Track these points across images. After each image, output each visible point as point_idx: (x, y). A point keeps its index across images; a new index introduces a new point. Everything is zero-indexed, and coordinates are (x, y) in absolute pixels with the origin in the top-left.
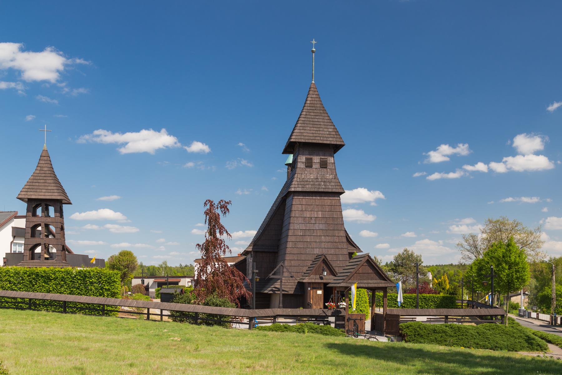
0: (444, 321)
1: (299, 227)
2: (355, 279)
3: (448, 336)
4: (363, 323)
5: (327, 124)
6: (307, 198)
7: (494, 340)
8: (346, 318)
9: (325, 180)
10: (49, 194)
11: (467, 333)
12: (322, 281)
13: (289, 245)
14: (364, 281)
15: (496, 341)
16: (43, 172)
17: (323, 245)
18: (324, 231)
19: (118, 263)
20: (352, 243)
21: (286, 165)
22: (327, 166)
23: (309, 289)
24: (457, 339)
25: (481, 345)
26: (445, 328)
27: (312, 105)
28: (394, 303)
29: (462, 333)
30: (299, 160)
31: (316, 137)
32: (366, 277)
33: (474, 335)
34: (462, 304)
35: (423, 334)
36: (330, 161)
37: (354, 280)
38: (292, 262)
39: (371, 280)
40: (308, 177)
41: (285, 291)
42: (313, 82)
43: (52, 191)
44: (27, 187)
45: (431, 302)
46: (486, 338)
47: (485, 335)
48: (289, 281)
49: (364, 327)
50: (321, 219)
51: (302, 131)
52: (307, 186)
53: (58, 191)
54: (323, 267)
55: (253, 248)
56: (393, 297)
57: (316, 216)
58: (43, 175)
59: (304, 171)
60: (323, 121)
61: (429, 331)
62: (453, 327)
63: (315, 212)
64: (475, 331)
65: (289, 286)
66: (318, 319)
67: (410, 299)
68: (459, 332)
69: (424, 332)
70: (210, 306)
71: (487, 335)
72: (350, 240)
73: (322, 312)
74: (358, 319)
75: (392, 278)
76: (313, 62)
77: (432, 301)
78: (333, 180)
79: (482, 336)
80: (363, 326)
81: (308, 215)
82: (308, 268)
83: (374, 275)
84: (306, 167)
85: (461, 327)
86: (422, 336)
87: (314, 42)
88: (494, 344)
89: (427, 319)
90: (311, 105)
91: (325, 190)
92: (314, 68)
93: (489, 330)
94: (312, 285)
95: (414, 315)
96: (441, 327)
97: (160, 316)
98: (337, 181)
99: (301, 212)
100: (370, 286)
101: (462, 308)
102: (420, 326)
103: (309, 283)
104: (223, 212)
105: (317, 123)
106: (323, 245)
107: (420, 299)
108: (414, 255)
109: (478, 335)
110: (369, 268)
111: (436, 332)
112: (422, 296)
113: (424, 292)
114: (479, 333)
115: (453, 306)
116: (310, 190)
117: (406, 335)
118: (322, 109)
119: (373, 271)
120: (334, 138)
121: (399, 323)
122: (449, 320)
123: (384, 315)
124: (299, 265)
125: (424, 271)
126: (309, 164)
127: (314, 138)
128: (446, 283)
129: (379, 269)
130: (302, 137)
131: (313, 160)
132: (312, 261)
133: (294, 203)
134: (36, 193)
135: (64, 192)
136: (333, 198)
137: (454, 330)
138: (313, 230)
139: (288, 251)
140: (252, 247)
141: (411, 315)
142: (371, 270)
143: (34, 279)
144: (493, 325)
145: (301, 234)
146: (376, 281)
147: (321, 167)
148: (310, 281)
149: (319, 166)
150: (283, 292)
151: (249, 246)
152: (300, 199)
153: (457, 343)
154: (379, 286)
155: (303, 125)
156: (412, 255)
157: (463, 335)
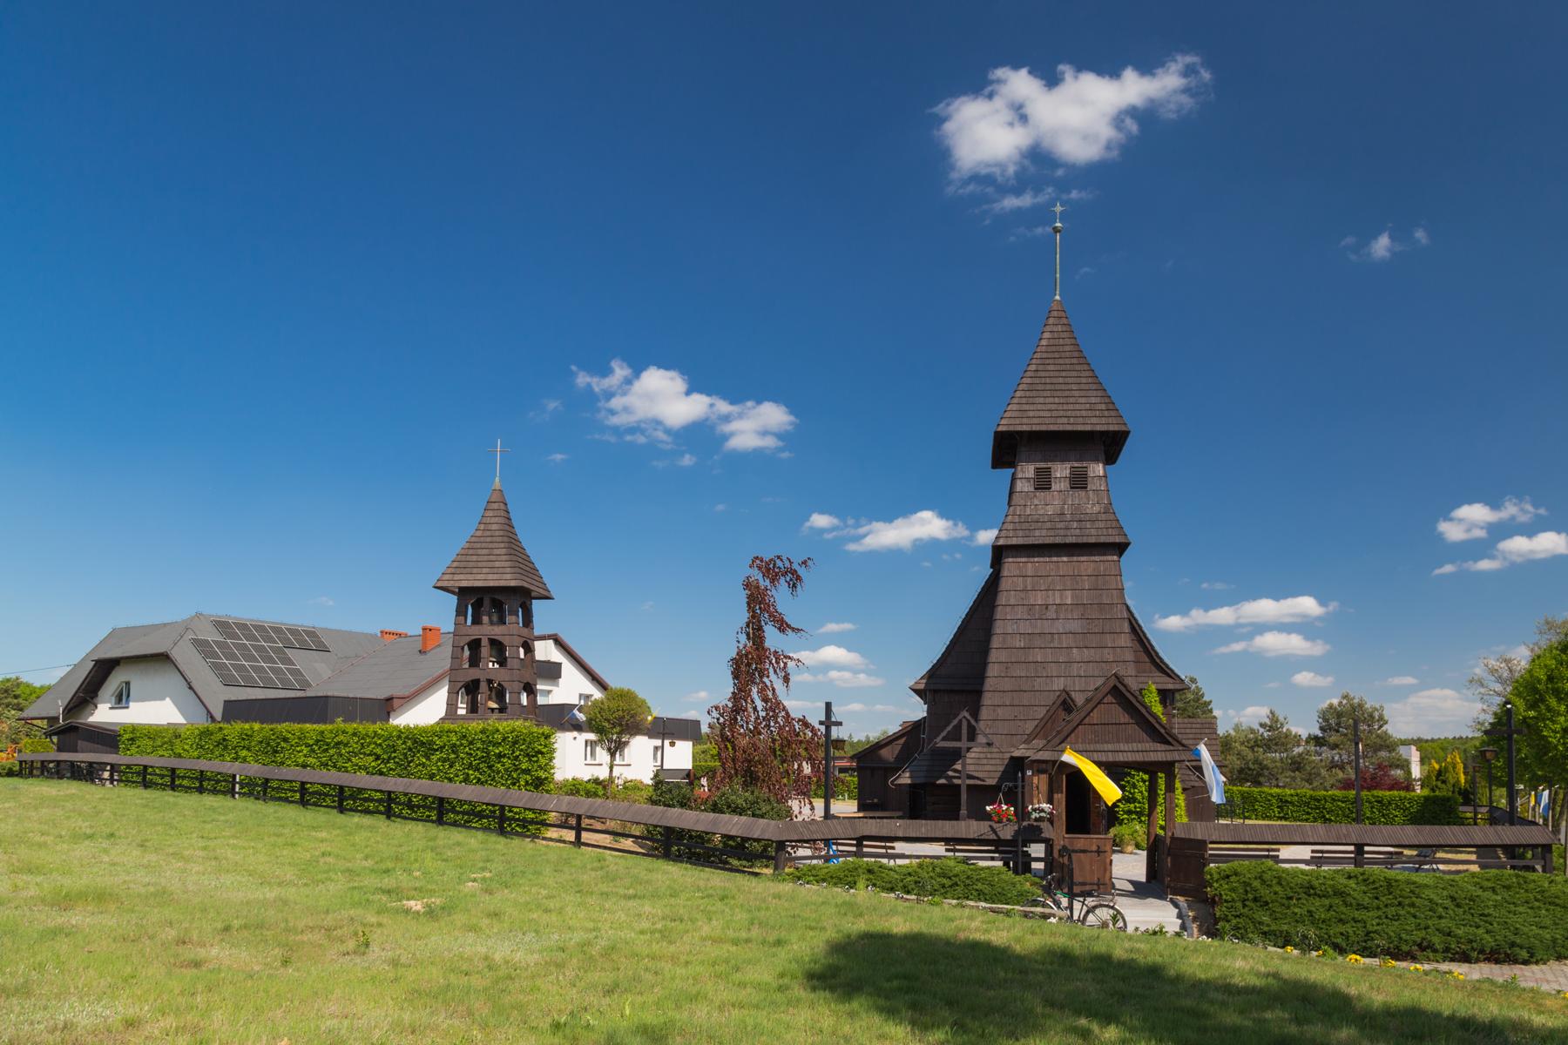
0: (1353, 861)
2: (1080, 740)
3: (1351, 905)
5: (1086, 387)
6: (1036, 559)
7: (1506, 922)
8: (1055, 847)
10: (495, 576)
11: (1414, 899)
13: (992, 670)
14: (1105, 745)
15: (1512, 925)
16: (488, 533)
17: (1075, 669)
18: (1078, 636)
19: (599, 716)
24: (1379, 917)
25: (1461, 938)
27: (1054, 349)
28: (1304, 811)
32: (1111, 735)
33: (1441, 904)
34: (1475, 815)
36: (1094, 472)
38: (1000, 711)
39: (1127, 742)
40: (1041, 512)
41: (978, 778)
42: (1058, 297)
43: (501, 570)
44: (455, 564)
46: (1481, 915)
47: (1478, 906)
48: (989, 756)
52: (1037, 533)
53: (513, 570)
58: (489, 539)
59: (1031, 499)
60: (1078, 380)
62: (1371, 880)
64: (1445, 893)
66: (1001, 848)
67: (1343, 802)
68: (1391, 893)
69: (1276, 893)
70: (722, 812)
71: (1483, 905)
72: (1158, 661)
73: (989, 829)
74: (1092, 852)
77: (1397, 806)
79: (1467, 909)
80: (1105, 870)
81: (1039, 599)
83: (1134, 730)
85: (1396, 881)
86: (1267, 903)
88: (1505, 937)
89: (1313, 851)
90: (1050, 349)
91: (1080, 540)
92: (1058, 267)
93: (1493, 890)
95: (1255, 840)
96: (1332, 879)
98: (1112, 517)
99: (1022, 595)
100: (1122, 759)
101: (1476, 824)
102: (1265, 876)
105: (1063, 387)
106: (1075, 669)
108: (1366, 706)
109: (1453, 907)
110: (1120, 709)
111: (1315, 894)
112: (1373, 796)
113: (1375, 788)
114: (1458, 901)
115: (1451, 820)
118: (1076, 354)
119: (1132, 718)
121: (1205, 865)
122: (1366, 856)
124: (1016, 716)
126: (1043, 482)
127: (1053, 421)
128: (1456, 770)
129: (1147, 711)
130: (1025, 421)
131: (1053, 473)
134: (469, 577)
135: (533, 571)
136: (1102, 558)
137: (1374, 889)
138: (1050, 636)
140: (924, 681)
142: (1126, 715)
143: (410, 749)
144: (1509, 875)
145: (1022, 645)
146: (1139, 745)
147: (1072, 488)
149: (1068, 486)
151: (922, 678)
153: (1378, 928)
154: (1146, 759)
155: (1028, 394)
156: (1360, 706)
157: (1400, 904)
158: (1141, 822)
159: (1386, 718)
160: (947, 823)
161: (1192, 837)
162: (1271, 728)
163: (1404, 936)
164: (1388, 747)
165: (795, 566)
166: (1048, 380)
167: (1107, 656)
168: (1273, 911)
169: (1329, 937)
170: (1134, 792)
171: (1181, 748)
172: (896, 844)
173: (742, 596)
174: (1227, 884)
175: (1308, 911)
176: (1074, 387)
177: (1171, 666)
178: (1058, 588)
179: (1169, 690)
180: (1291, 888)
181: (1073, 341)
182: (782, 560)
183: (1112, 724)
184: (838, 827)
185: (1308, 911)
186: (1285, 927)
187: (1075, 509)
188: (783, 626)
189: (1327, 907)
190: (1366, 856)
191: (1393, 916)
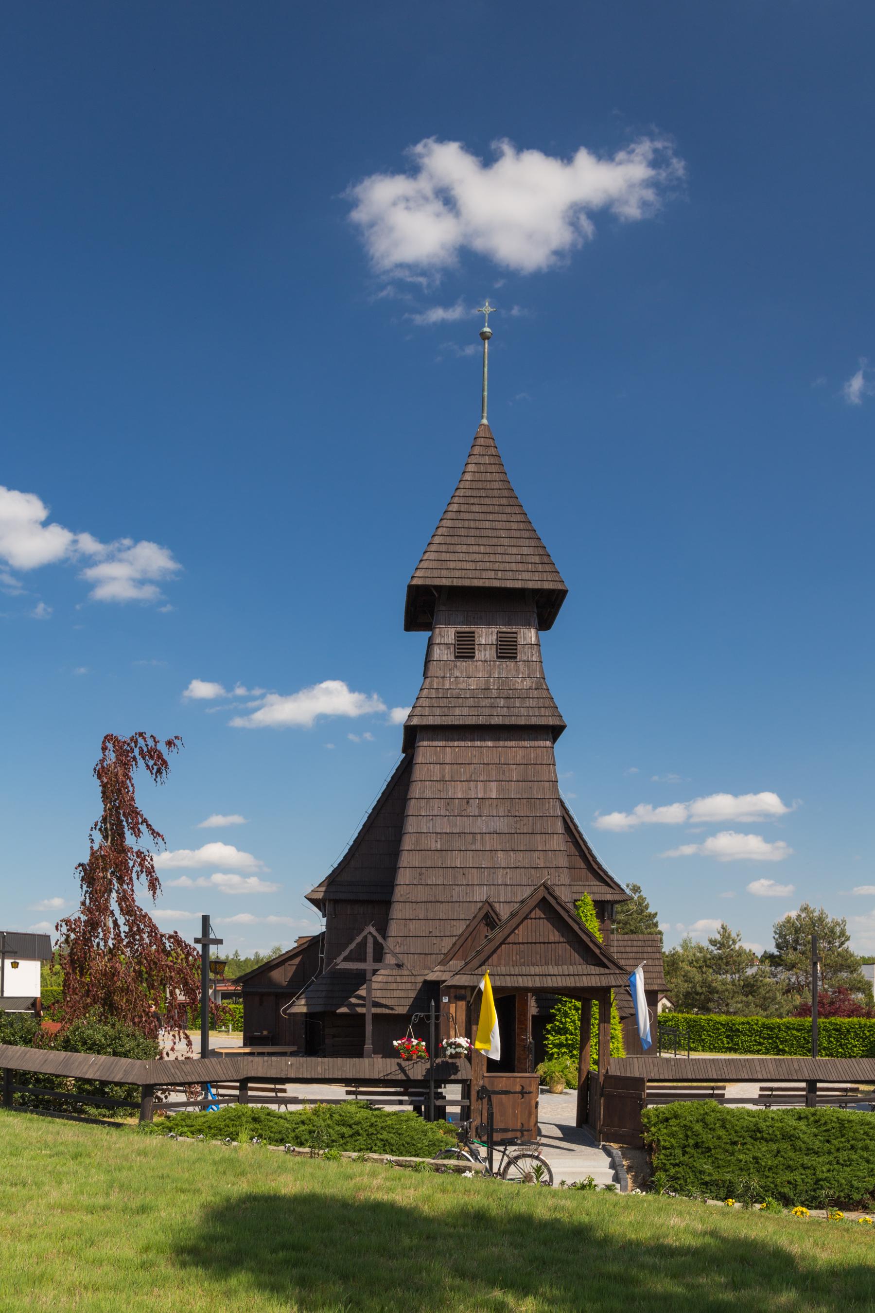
0: (804, 1099)
1: (434, 826)
2: (503, 962)
4: (530, 1103)
5: (518, 534)
6: (456, 744)
13: (403, 877)
14: (532, 968)
20: (601, 873)
22: (516, 653)
23: (445, 1000)
24: (830, 1163)
26: (794, 1123)
28: (755, 1041)
29: (853, 1142)
31: (484, 572)
32: (538, 957)
36: (525, 639)
37: (499, 965)
38: (412, 925)
40: (462, 686)
41: (386, 1006)
45: (854, 1039)
48: (399, 979)
49: (533, 1117)
50: (495, 802)
52: (457, 711)
55: (325, 892)
56: (754, 1026)
59: (450, 670)
61: (736, 1132)
62: (823, 1122)
63: (480, 785)
65: (397, 994)
66: (411, 1090)
67: (798, 1030)
68: (843, 1136)
69: (719, 1138)
72: (596, 867)
73: (397, 1068)
74: (515, 1093)
75: (765, 977)
76: (484, 366)
78: (535, 693)
80: (530, 1114)
83: (565, 950)
84: (456, 657)
85: (850, 1121)
86: (709, 1149)
89: (762, 1089)
90: (474, 485)
91: (507, 721)
92: (486, 383)
95: (698, 1077)
96: (781, 1121)
98: (545, 694)
99: (439, 786)
100: (550, 985)
104: (154, 771)
105: (490, 533)
107: (824, 1030)
108: (827, 920)
110: (550, 926)
111: (762, 1138)
112: (831, 1023)
113: (834, 1014)
117: (657, 1145)
118: (506, 493)
120: (536, 574)
121: (642, 1106)
122: (818, 1093)
124: (430, 932)
125: (849, 961)
127: (477, 574)
129: (580, 928)
130: (444, 573)
139: (401, 895)
140: (323, 889)
141: (690, 1077)
142: (556, 933)
145: (439, 847)
147: (498, 657)
150: (378, 1010)
151: (320, 886)
152: (438, 748)
154: (578, 985)
155: (448, 540)
156: (821, 920)
157: (852, 1147)
159: (848, 934)
161: (629, 1075)
162: (722, 946)
163: (855, 1183)
164: (849, 967)
165: (162, 747)
166: (472, 524)
168: (716, 1158)
169: (776, 1186)
171: (617, 971)
172: (288, 1086)
174: (666, 1128)
176: (503, 534)
178: (481, 778)
179: (608, 902)
181: (502, 477)
182: (144, 739)
184: (218, 1067)
186: (728, 1177)
187: (503, 682)
189: (775, 1153)
190: (818, 1093)
191: (845, 1161)
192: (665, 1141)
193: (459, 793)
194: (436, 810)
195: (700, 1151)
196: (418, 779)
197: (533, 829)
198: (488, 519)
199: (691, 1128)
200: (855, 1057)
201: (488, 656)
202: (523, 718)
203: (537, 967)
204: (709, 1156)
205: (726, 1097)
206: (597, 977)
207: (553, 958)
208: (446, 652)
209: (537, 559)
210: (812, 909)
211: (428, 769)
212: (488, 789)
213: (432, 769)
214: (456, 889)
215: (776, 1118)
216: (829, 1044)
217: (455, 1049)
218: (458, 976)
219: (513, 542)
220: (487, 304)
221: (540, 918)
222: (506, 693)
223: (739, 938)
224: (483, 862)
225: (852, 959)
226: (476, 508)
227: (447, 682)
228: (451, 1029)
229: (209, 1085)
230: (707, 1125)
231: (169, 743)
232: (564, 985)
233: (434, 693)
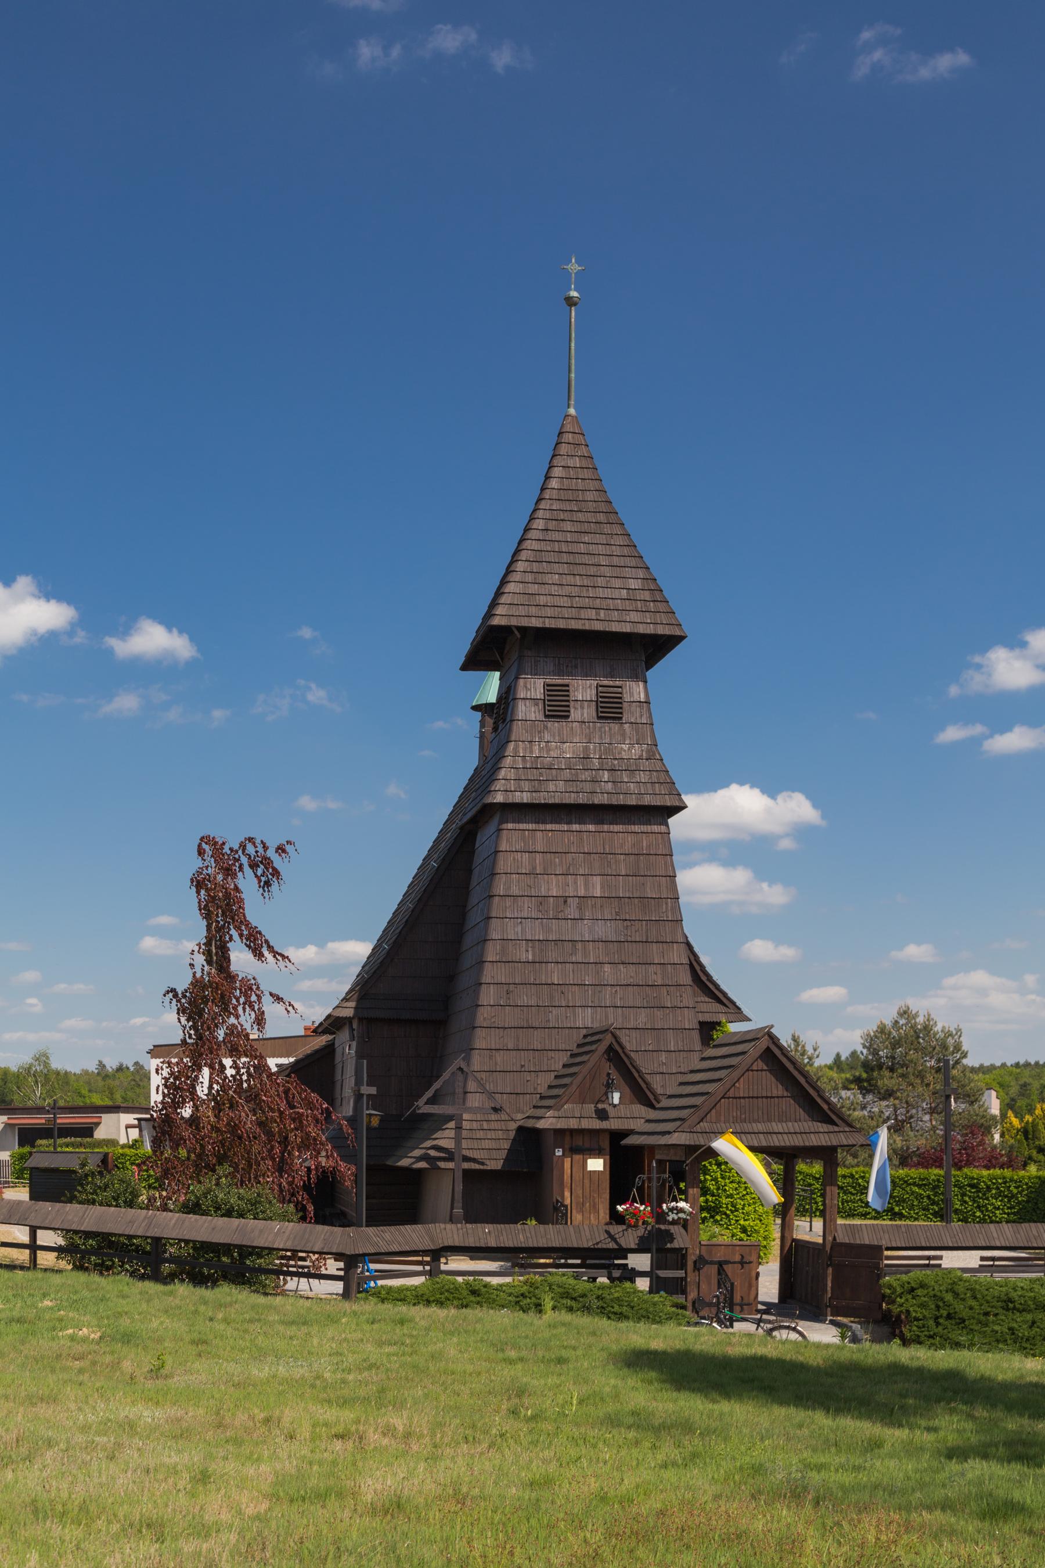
2: (722, 1119)
5: (622, 561)
6: (549, 827)
9: (616, 762)
12: (604, 1125)
13: (488, 996)
14: (754, 1125)
17: (607, 996)
18: (611, 945)
21: (476, 708)
23: (559, 1152)
30: (521, 694)
31: (582, 611)
32: (760, 1113)
35: (965, 1314)
36: (631, 694)
37: (718, 1121)
38: (499, 1057)
40: (553, 754)
41: (474, 1160)
45: (996, 1199)
48: (485, 1125)
49: (753, 1289)
51: (534, 589)
52: (551, 786)
54: (609, 1074)
55: (356, 1008)
56: (860, 1181)
57: (582, 893)
59: (539, 732)
61: (988, 1302)
63: (580, 880)
65: (486, 1144)
66: (588, 1262)
67: (919, 1186)
69: (971, 1308)
72: (704, 978)
73: (606, 1236)
78: (645, 764)
80: (750, 1286)
81: (553, 887)
82: (556, 1077)
83: (790, 1105)
84: (546, 716)
87: (574, 267)
89: (982, 1259)
94: (567, 1138)
95: (933, 1245)
96: (1031, 1290)
97: (39, 1243)
100: (777, 1144)
102: (956, 1287)
103: (559, 1133)
105: (586, 559)
107: (955, 1186)
110: (773, 1079)
116: (562, 799)
117: (906, 1317)
118: (603, 507)
120: (647, 614)
121: (879, 1277)
123: (828, 1248)
124: (522, 1066)
129: (807, 1082)
130: (533, 610)
131: (571, 694)
132: (569, 1053)
133: (503, 846)
139: (484, 1019)
140: (353, 1004)
141: (924, 1244)
142: (780, 1087)
145: (530, 958)
147: (599, 718)
148: (561, 1124)
149: (594, 714)
150: (466, 1165)
151: (345, 999)
154: (807, 1144)
155: (535, 567)
156: (927, 1028)
158: (716, 1222)
159: (964, 1048)
160: (408, 1229)
161: (858, 1242)
164: (969, 1096)
165: (271, 853)
167: (654, 977)
170: (706, 1180)
171: (847, 1129)
173: (191, 899)
174: (913, 1298)
175: (1009, 1329)
177: (723, 987)
178: (581, 872)
180: (988, 1302)
182: (254, 844)
183: (762, 1097)
184: (414, 1236)
185: (1009, 1329)
187: (605, 749)
188: (256, 943)
189: (1030, 1323)
192: (916, 1312)
193: (555, 890)
194: (526, 911)
195: (954, 1322)
196: (502, 871)
197: (647, 937)
198: (583, 540)
199: (942, 1299)
200: (998, 1222)
201: (585, 715)
202: (634, 796)
203: (759, 1124)
204: (963, 1328)
205: (943, 1266)
206: (826, 1135)
207: (776, 1114)
208: (533, 709)
209: (647, 596)
210: (913, 1012)
211: (514, 859)
212: (591, 885)
213: (520, 859)
214: (554, 1012)
215: (1025, 1287)
216: (961, 1205)
217: (677, 1214)
218: (677, 1134)
219: (617, 572)
220: (573, 261)
221: (762, 1070)
222: (610, 764)
223: (817, 1053)
224: (587, 978)
225: (972, 1085)
226: (568, 526)
227: (536, 748)
228: (566, 1189)
229: (366, 1258)
230: (958, 1294)
231: (281, 850)
232: (793, 1144)
233: (520, 761)
